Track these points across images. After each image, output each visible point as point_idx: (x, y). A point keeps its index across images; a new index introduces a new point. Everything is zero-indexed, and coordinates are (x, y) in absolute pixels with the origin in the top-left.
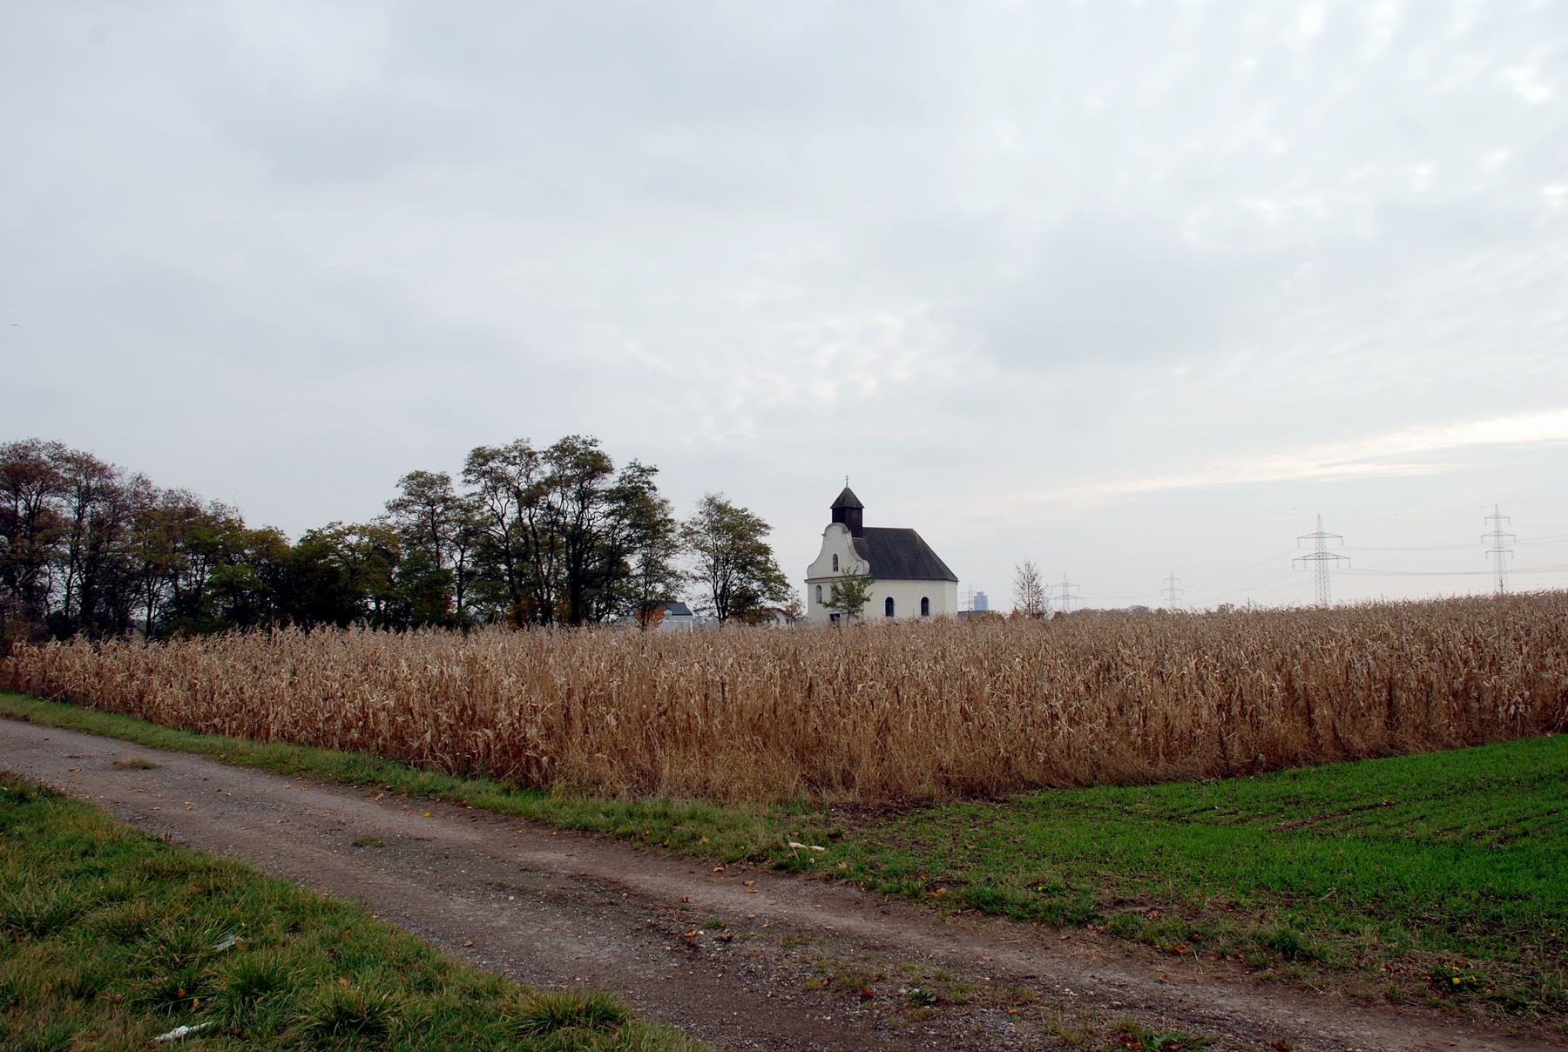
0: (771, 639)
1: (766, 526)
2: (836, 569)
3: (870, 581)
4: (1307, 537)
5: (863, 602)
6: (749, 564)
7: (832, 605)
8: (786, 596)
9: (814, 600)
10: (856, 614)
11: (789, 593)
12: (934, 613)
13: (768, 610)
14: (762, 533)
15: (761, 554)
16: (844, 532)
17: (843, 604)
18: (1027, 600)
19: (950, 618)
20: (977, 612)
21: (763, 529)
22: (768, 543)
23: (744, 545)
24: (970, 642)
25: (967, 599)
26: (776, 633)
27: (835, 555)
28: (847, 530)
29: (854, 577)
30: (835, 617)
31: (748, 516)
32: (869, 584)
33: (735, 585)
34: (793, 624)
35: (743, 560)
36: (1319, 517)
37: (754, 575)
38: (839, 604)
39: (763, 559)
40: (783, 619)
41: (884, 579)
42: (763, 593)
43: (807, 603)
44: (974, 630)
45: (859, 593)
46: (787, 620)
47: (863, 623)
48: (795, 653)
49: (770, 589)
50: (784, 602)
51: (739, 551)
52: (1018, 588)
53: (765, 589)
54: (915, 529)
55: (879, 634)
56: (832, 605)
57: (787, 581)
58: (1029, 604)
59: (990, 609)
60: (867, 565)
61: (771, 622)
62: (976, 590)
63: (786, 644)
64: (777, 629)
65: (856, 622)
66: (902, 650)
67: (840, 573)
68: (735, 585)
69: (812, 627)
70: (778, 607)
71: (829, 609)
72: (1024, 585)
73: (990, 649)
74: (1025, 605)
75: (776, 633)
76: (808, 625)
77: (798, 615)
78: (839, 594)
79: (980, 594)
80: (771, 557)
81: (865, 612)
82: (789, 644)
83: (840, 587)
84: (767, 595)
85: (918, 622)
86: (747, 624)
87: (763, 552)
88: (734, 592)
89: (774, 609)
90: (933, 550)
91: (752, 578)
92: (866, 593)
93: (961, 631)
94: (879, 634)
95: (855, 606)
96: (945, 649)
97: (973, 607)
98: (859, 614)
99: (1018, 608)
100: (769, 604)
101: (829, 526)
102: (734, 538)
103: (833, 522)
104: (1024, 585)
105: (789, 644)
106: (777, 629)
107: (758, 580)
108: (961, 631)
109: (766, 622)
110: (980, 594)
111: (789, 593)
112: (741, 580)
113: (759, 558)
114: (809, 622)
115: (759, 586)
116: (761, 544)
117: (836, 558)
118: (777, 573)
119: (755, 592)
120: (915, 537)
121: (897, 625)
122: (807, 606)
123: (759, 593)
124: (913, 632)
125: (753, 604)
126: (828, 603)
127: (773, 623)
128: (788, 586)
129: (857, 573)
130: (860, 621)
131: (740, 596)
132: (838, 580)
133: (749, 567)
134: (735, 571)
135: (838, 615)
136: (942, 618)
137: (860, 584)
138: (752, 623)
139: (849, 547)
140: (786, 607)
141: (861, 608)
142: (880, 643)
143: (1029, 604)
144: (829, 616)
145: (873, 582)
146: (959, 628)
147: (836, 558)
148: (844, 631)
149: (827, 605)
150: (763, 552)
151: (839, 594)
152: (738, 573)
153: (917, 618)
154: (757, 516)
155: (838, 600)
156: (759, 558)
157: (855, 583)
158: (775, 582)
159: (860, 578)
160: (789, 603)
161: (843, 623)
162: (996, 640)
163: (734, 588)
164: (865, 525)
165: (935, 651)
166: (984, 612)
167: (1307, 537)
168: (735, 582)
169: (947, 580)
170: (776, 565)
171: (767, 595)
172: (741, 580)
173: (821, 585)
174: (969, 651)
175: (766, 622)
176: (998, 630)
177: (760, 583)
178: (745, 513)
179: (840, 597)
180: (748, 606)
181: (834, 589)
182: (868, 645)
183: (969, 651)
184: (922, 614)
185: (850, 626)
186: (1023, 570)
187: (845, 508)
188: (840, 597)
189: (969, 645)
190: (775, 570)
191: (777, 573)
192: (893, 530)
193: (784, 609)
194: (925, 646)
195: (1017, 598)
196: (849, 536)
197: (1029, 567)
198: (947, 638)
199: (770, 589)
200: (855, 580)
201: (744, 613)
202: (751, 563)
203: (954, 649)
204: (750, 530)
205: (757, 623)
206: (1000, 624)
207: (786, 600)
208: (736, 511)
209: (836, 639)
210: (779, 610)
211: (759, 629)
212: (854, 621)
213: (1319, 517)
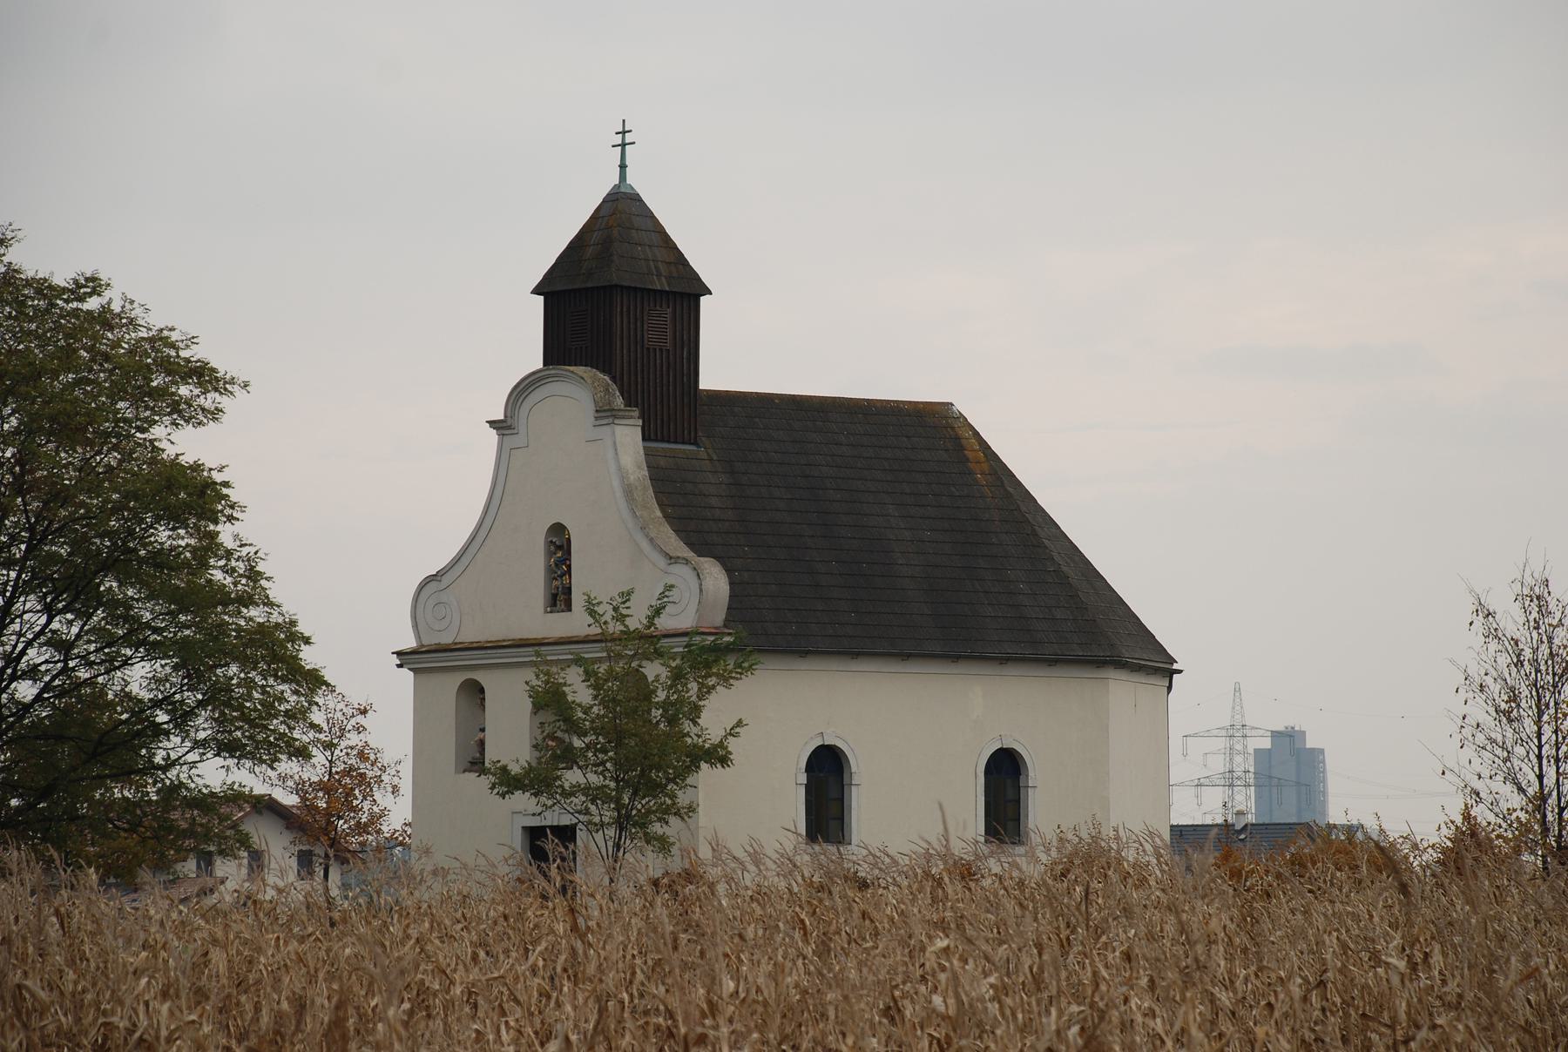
0: (217, 956)
1: (203, 375)
2: (560, 598)
3: (731, 661)
4: (1207, 734)
5: (693, 766)
6: (107, 567)
7: (537, 781)
8: (301, 735)
9: (447, 750)
10: (657, 828)
11: (317, 717)
12: (1051, 835)
13: (206, 802)
14: (181, 412)
15: (175, 517)
16: (605, 413)
17: (594, 779)
18: (1528, 775)
19: (1130, 855)
20: (1267, 833)
21: (184, 391)
22: (209, 461)
23: (85, 467)
24: (1230, 984)
25: (1218, 765)
26: (243, 925)
27: (558, 529)
28: (619, 402)
29: (649, 642)
30: (550, 844)
31: (105, 319)
32: (726, 680)
33: (33, 673)
34: (335, 876)
35: (78, 545)
36: (1237, 690)
37: (136, 625)
38: (573, 777)
39: (185, 540)
40: (279, 848)
41: (804, 653)
42: (182, 718)
43: (407, 770)
44: (1249, 921)
45: (672, 721)
46: (305, 860)
47: (689, 876)
48: (338, 1023)
49: (219, 696)
50: (288, 766)
51: (58, 496)
52: (1480, 712)
53: (191, 698)
54: (963, 406)
55: (770, 928)
56: (537, 781)
57: (309, 657)
58: (1542, 798)
59: (1336, 815)
60: (717, 581)
61: (223, 867)
62: (1267, 719)
63: (293, 981)
64: (249, 902)
65: (650, 864)
66: (886, 1012)
67: (575, 623)
68: (33, 673)
69: (431, 892)
70: (260, 789)
71: (523, 801)
72: (1514, 698)
73: (1334, 1020)
74: (1517, 801)
75: (243, 925)
76: (413, 881)
77: (361, 828)
78: (574, 727)
79: (1288, 739)
80: (226, 534)
81: (703, 818)
82: (312, 979)
83: (580, 692)
84: (203, 726)
85: (967, 873)
86: (93, 875)
87: (188, 508)
88: (26, 708)
89: (236, 797)
90: (454, 745)
91: (126, 640)
92: (713, 720)
93: (1183, 928)
94: (770, 928)
95: (655, 788)
96: (1102, 1015)
97: (1246, 804)
98: (672, 828)
99: (1482, 814)
100: (213, 774)
101: (523, 390)
102: (28, 430)
103: (548, 360)
104: (1514, 698)
105: (312, 979)
106: (249, 902)
107: (154, 650)
108: (1183, 928)
109: (190, 866)
110: (1288, 739)
111: (317, 717)
112: (63, 646)
113: (163, 535)
114: (417, 864)
115: (158, 681)
116: (174, 463)
117: (559, 544)
118: (256, 613)
119: (139, 709)
120: (957, 439)
121: (863, 885)
122: (406, 786)
123: (162, 717)
124: (942, 926)
125: (125, 774)
126: (515, 769)
127: (231, 872)
128: (314, 681)
129: (665, 623)
130: (676, 864)
131: (54, 733)
132: (563, 653)
133: (110, 583)
134: (32, 602)
135: (566, 834)
136: (1088, 861)
137: (678, 676)
138: (121, 875)
139: (629, 492)
140: (300, 788)
141: (683, 798)
142: (776, 976)
143: (1542, 798)
144: (518, 840)
145: (742, 670)
146: (1172, 908)
147: (559, 544)
148: (593, 911)
149: (508, 782)
150: (188, 508)
151: (574, 727)
152: (50, 611)
153: (959, 849)
154: (155, 319)
155: (569, 757)
156: (163, 535)
157: (653, 670)
158: (247, 663)
159: (678, 646)
160: (316, 768)
161: (589, 873)
162: (1364, 976)
163: (26, 690)
164: (710, 379)
165: (1052, 1021)
166: (1308, 830)
167: (1207, 734)
168: (34, 655)
169: (1120, 664)
170: (254, 575)
171: (203, 726)
172: (63, 646)
173: (481, 677)
174: (1226, 1026)
175: (190, 866)
176: (1380, 926)
177: (162, 667)
178: (93, 304)
179: (578, 743)
180: (100, 780)
181: (549, 700)
182: (712, 982)
183: (1226, 1026)
184: (991, 831)
185: (625, 890)
186: (1512, 620)
187: (610, 289)
188: (578, 743)
189: (1224, 998)
190: (246, 600)
191: (256, 613)
192: (870, 403)
193: (290, 800)
194: (1001, 991)
195: (1476, 765)
196: (628, 438)
197: (1543, 610)
198: (1115, 957)
199: (219, 696)
200: (659, 654)
201: (74, 818)
202: (122, 562)
203: (1151, 1014)
204: (116, 393)
205: (145, 875)
206: (1383, 893)
207: (302, 753)
208: (44, 288)
209: (550, 955)
210: (266, 806)
211: (154, 902)
212: (646, 863)
213: (1237, 690)
